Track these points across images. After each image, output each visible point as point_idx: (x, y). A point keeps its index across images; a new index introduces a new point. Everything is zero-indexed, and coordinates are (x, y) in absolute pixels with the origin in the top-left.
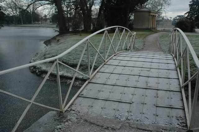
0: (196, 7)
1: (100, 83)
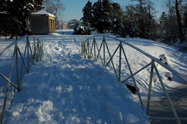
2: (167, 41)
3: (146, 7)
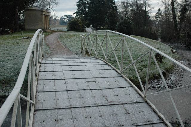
0: (83, 7)
1: (51, 108)
2: (166, 39)
3: (142, 3)
